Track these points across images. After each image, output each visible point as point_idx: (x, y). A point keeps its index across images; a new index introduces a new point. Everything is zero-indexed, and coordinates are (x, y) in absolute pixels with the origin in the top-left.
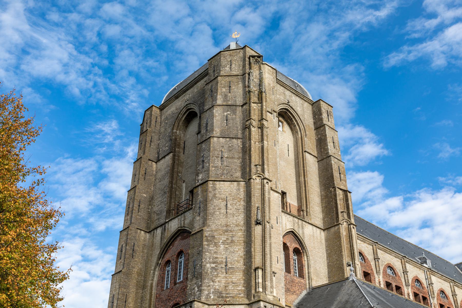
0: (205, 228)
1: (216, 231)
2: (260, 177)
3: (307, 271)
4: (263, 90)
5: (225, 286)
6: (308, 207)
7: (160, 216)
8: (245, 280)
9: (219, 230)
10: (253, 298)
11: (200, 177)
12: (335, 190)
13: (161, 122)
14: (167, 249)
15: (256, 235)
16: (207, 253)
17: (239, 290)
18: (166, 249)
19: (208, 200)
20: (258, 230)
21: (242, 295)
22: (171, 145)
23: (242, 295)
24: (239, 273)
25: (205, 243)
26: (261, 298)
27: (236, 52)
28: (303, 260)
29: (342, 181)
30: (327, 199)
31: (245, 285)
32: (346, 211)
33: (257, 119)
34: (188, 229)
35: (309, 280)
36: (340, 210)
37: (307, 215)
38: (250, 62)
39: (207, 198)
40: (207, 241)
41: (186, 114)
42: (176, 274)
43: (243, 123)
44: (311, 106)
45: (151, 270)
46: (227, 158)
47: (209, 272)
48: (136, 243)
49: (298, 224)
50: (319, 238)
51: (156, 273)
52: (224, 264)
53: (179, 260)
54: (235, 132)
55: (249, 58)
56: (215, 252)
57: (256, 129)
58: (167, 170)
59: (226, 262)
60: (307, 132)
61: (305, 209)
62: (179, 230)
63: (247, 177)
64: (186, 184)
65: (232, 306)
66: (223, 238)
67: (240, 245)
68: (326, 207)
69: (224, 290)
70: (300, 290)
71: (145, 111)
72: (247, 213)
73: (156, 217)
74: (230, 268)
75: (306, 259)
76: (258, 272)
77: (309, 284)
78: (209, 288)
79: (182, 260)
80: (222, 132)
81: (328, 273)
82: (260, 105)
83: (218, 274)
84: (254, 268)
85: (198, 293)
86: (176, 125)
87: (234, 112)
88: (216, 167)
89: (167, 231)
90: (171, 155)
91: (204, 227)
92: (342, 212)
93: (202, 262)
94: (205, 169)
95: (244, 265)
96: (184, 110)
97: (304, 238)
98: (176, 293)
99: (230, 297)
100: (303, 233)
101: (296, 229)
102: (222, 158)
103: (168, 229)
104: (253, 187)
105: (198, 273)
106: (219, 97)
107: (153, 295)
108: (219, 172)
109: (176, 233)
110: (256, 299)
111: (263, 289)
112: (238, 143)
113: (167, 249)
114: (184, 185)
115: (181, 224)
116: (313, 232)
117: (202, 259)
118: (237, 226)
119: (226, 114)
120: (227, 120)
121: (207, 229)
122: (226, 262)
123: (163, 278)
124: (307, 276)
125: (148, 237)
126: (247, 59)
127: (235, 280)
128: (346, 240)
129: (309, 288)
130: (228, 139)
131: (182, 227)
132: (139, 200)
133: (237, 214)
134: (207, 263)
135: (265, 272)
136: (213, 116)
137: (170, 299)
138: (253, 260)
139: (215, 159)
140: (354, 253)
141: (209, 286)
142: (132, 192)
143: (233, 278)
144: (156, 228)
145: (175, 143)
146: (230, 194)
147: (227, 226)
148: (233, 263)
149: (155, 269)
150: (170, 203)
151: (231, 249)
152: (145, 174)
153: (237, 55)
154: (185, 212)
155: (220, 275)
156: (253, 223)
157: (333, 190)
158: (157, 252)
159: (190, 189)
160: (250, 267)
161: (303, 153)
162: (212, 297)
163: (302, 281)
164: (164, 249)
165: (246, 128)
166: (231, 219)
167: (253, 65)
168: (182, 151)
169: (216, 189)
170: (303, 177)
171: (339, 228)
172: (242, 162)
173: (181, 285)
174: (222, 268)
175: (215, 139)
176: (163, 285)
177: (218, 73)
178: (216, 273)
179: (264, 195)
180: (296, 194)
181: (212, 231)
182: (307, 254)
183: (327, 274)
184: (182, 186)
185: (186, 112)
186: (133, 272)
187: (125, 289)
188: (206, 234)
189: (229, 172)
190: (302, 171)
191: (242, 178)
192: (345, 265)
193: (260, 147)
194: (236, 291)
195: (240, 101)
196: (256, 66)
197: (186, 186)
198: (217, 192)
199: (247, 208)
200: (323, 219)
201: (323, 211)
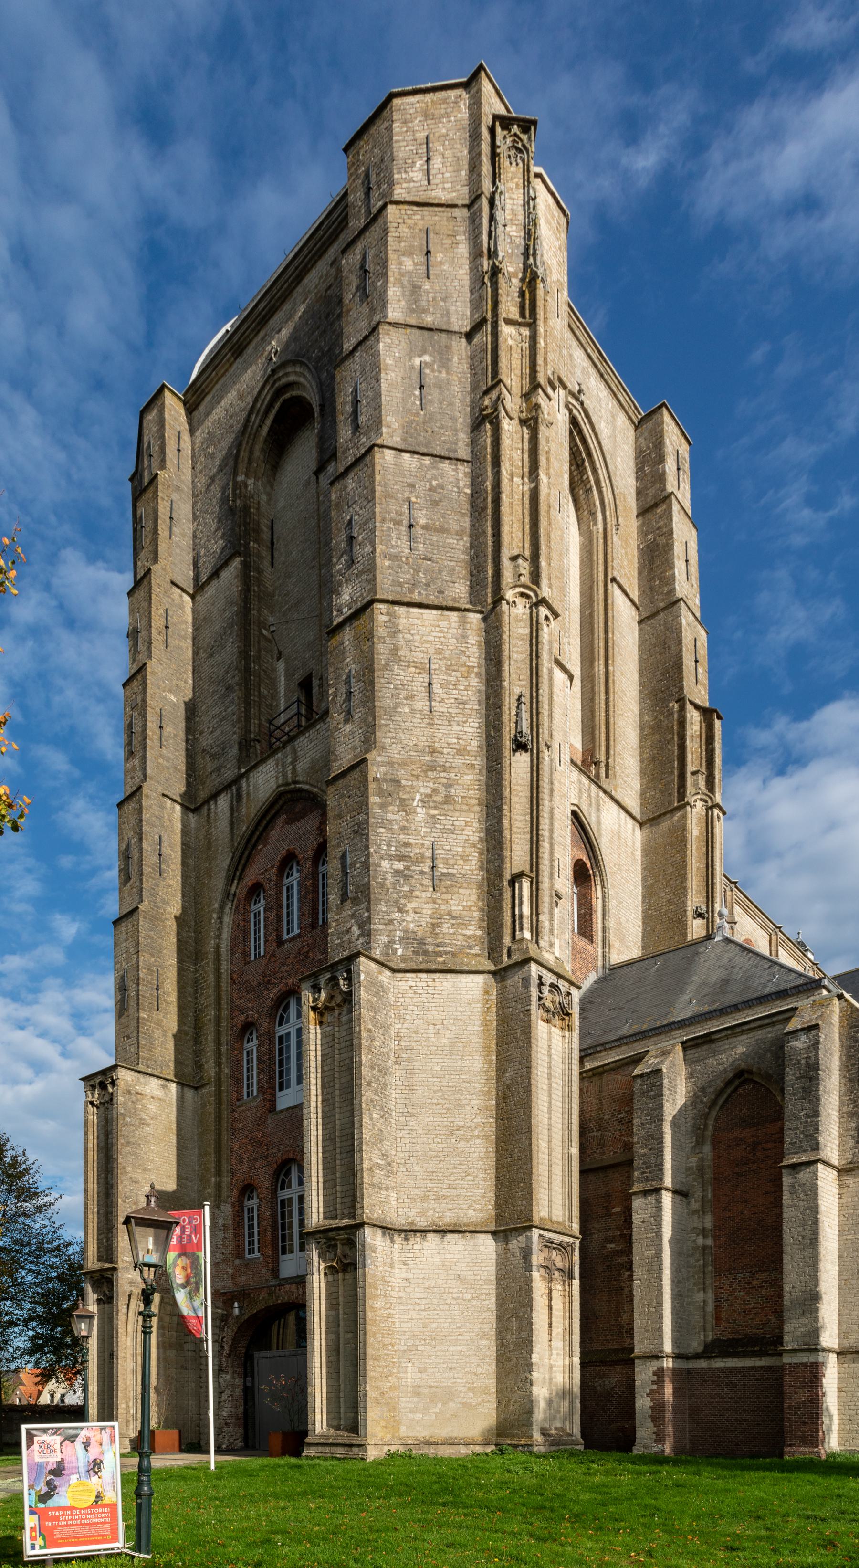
0: (372, 756)
1: (403, 764)
2: (528, 597)
3: (600, 926)
4: (540, 272)
5: (433, 925)
6: (612, 752)
7: (222, 760)
8: (482, 910)
9: (412, 762)
10: (505, 958)
11: (346, 597)
12: (682, 708)
13: (193, 456)
14: (250, 853)
15: (513, 782)
16: (382, 830)
17: (469, 937)
18: (247, 853)
19: (376, 666)
20: (518, 765)
21: (476, 950)
22: (232, 529)
23: (476, 950)
24: (468, 891)
25: (374, 799)
26: (532, 954)
27: (445, 101)
28: (593, 894)
29: (699, 687)
30: (657, 737)
31: (485, 924)
32: (704, 769)
33: (516, 390)
34: (307, 787)
35: (604, 948)
36: (690, 768)
37: (607, 776)
38: (494, 146)
39: (372, 665)
40: (380, 793)
41: (274, 411)
42: (279, 918)
43: (472, 401)
44: (631, 429)
45: (213, 911)
46: (426, 527)
47: (388, 882)
48: (164, 838)
49: (589, 796)
50: (630, 844)
51: (227, 919)
52: (429, 863)
53: (286, 881)
54: (447, 436)
55: (492, 131)
56: (403, 828)
57: (516, 422)
58: (227, 614)
59: (433, 858)
60: (620, 520)
61: (603, 759)
62: (280, 795)
63: (487, 600)
64: (286, 663)
65: (453, 975)
66: (424, 788)
67: (469, 811)
68: (653, 759)
69: (428, 934)
70: (584, 970)
71: (143, 414)
72: (487, 716)
73: (210, 766)
74: (442, 874)
75: (600, 895)
76: (521, 888)
77: (604, 956)
78: (391, 927)
79: (294, 879)
80: (408, 429)
81: (644, 936)
82: (526, 332)
83: (411, 891)
84: (509, 877)
85: (361, 941)
86: (244, 454)
87: (444, 357)
88: (394, 557)
89: (244, 800)
90: (236, 562)
91: (368, 751)
92: (693, 773)
93: (368, 856)
94: (355, 569)
95: (481, 868)
96: (267, 395)
97: (600, 835)
98: (283, 964)
99: (446, 953)
100: (599, 823)
101: (584, 808)
102: (411, 526)
103: (248, 794)
104: (506, 629)
105: (358, 887)
106: (393, 292)
107: (224, 976)
108: (404, 577)
109: (272, 805)
110: (517, 957)
111: (532, 932)
112: (456, 478)
113: (250, 853)
114: (281, 666)
115: (285, 776)
116: (620, 826)
117: (367, 847)
118: (459, 752)
119: (417, 361)
120: (421, 387)
121: (379, 759)
122: (433, 858)
123: (246, 932)
124: (600, 938)
125: (193, 826)
126: (486, 135)
127: (456, 909)
128: (697, 849)
129: (604, 967)
130: (427, 461)
131: (288, 784)
132: (158, 710)
133: (460, 718)
134: (382, 858)
135: (537, 889)
136: (375, 368)
137: (269, 982)
138: (507, 853)
139: (389, 528)
140: (713, 884)
141: (391, 922)
142: (135, 683)
143: (452, 902)
144: (214, 796)
145: (246, 524)
146: (438, 652)
147: (433, 752)
148: (452, 862)
149: (222, 908)
150: (248, 718)
151: (447, 822)
152: (167, 627)
153: (448, 115)
154: (292, 739)
155: (417, 893)
156: (507, 744)
157: (676, 706)
158: (224, 861)
159: (298, 677)
160: (500, 875)
161: (606, 585)
162: (399, 952)
163: (589, 947)
164: (243, 853)
165: (484, 419)
166: (444, 730)
167: (504, 162)
168: (265, 553)
169: (398, 631)
170: (602, 662)
171: (684, 817)
172: (471, 547)
173: (298, 944)
174: (422, 873)
175: (389, 454)
176: (247, 949)
177: (383, 195)
178: (406, 888)
179: (537, 657)
180: (580, 713)
181: (391, 764)
182: (602, 881)
183: (640, 938)
184: (274, 670)
185: (271, 405)
186: (167, 916)
187: (153, 956)
188: (376, 770)
189: (434, 579)
190: (602, 644)
191: (471, 602)
192: (690, 914)
193: (527, 497)
194: (460, 937)
195: (460, 316)
196: (513, 168)
197: (287, 670)
198: (402, 642)
199: (488, 698)
200: (641, 795)
201: (643, 773)
